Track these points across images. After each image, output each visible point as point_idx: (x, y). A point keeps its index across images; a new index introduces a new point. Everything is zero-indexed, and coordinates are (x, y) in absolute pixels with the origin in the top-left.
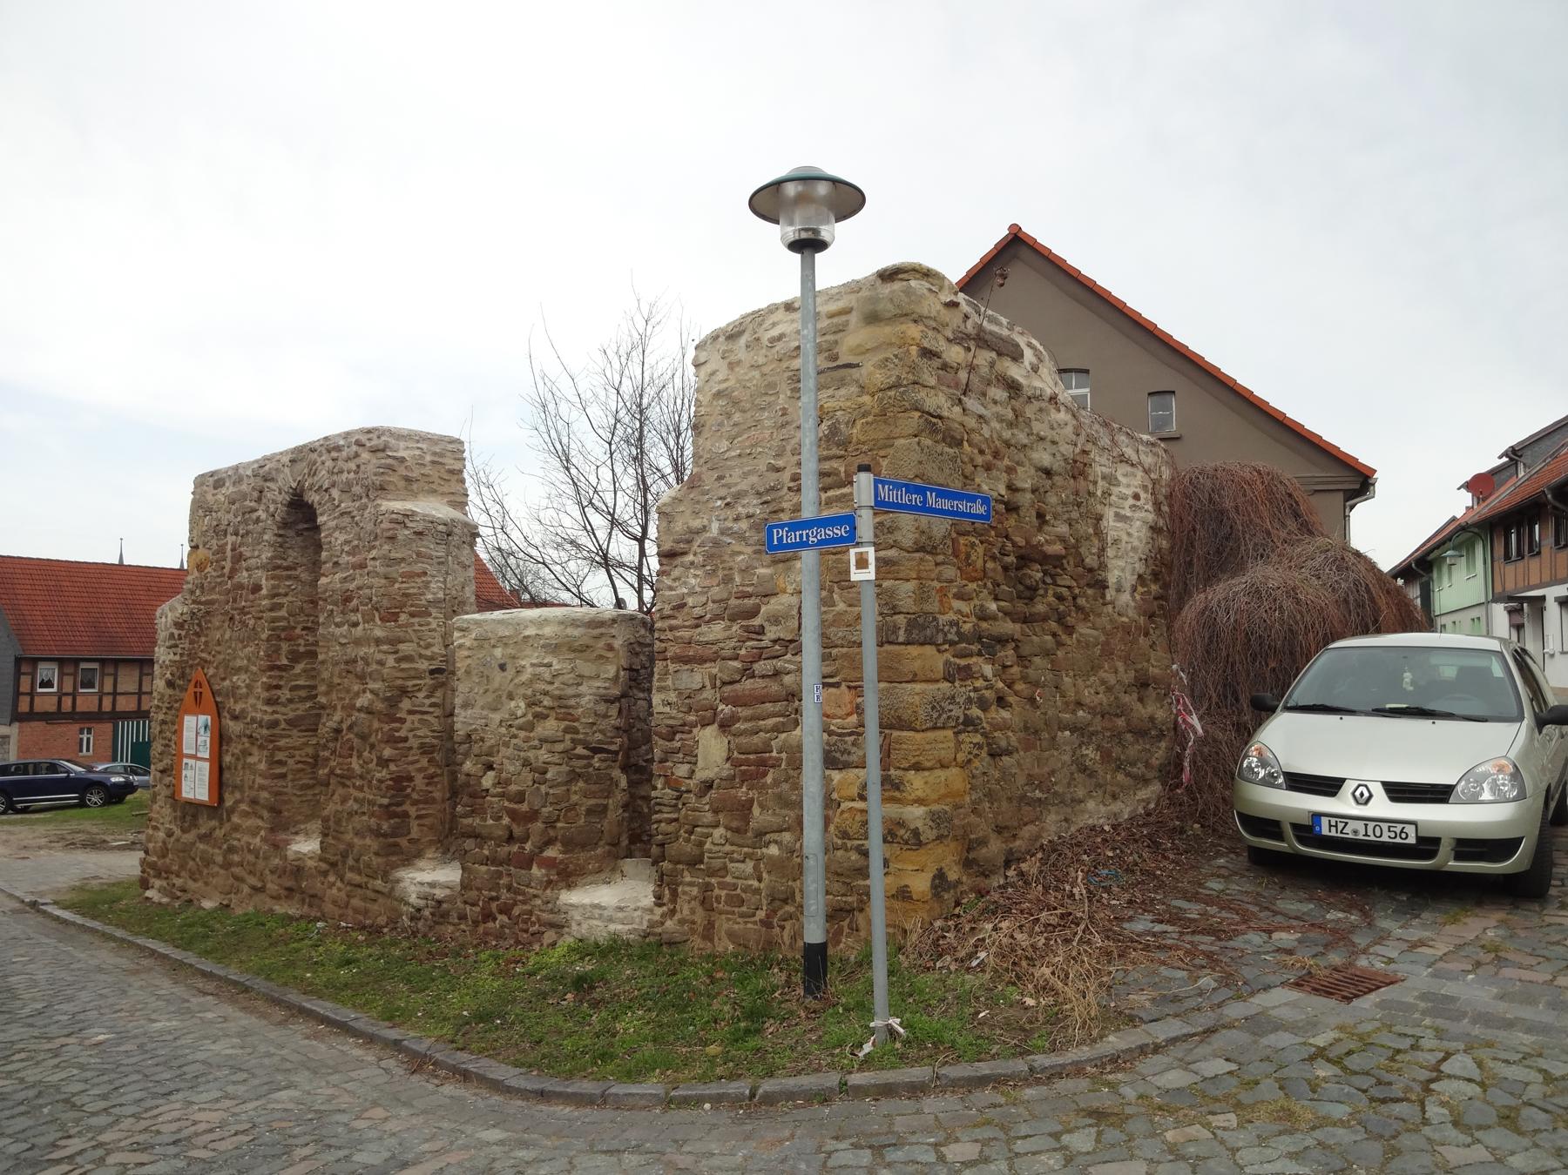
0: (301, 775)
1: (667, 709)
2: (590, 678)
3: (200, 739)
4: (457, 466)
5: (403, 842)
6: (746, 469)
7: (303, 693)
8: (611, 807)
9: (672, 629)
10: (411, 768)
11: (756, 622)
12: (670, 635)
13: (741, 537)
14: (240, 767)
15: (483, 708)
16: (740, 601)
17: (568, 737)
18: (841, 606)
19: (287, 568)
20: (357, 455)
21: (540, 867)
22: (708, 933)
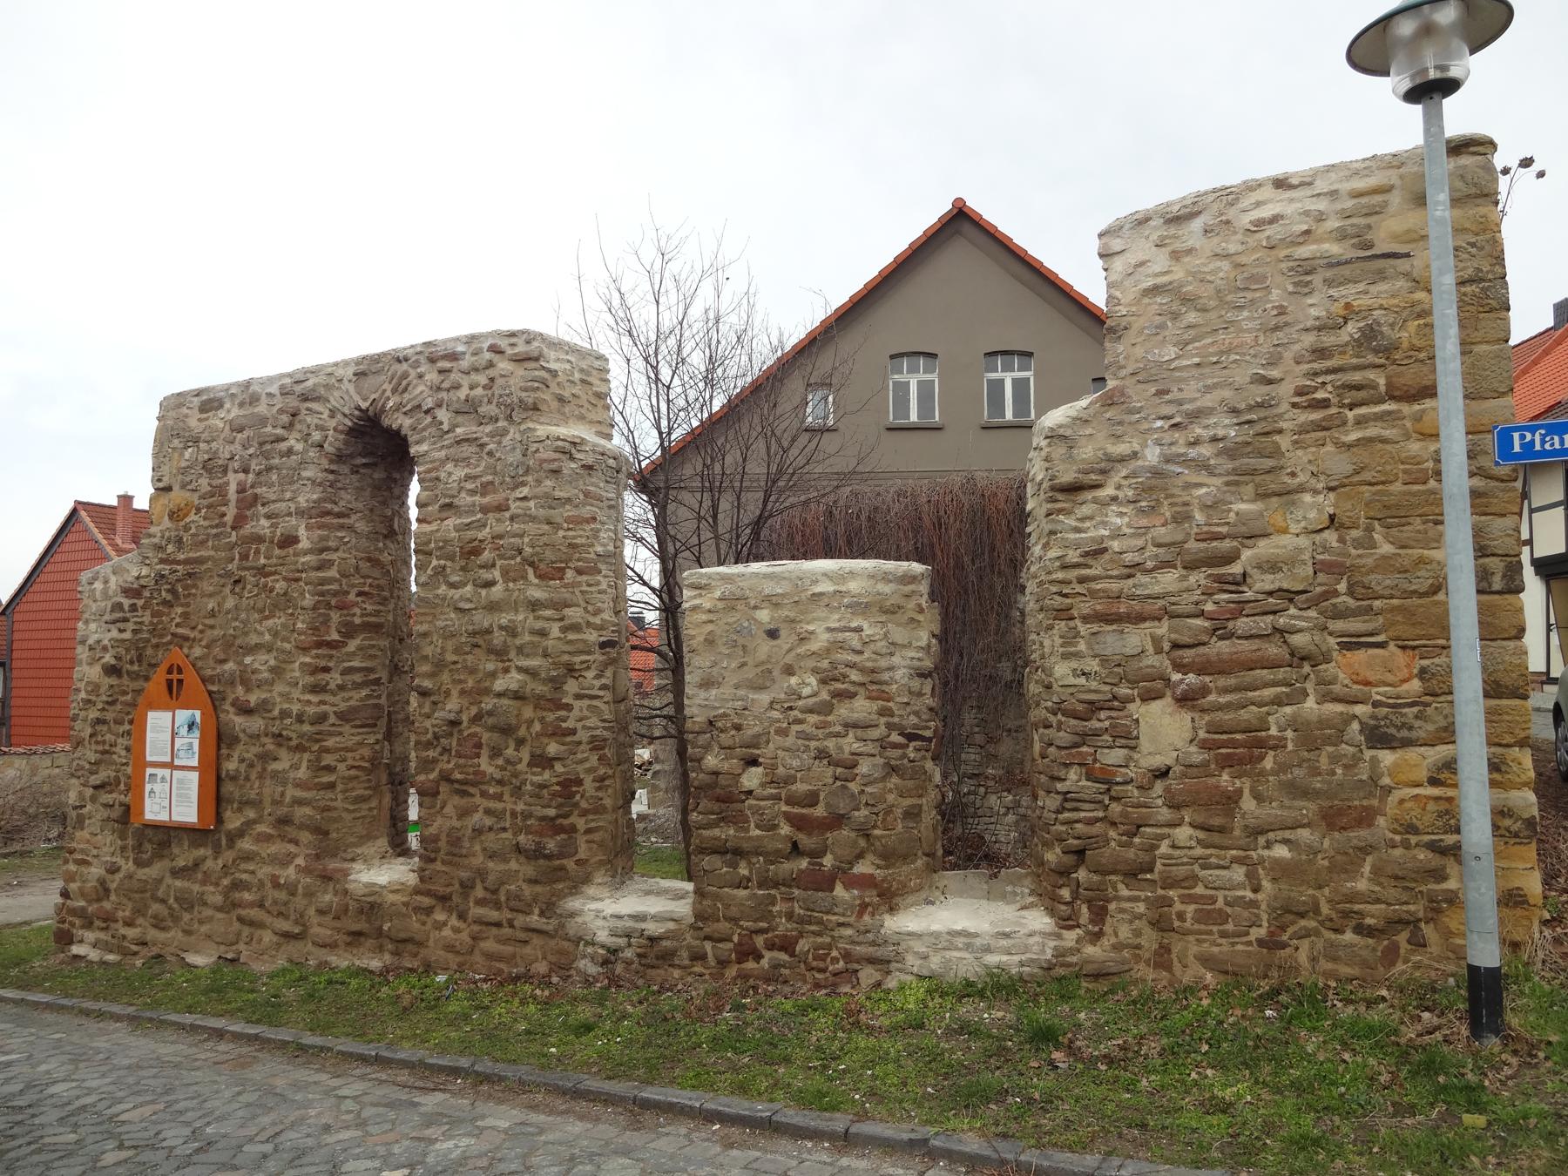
0: (354, 784)
1: (1082, 680)
2: (904, 646)
3: (178, 742)
4: (602, 389)
5: (570, 864)
6: (1209, 382)
7: (358, 678)
8: (925, 808)
9: (1082, 580)
10: (580, 768)
11: (1236, 569)
12: (1079, 588)
13: (1202, 466)
14: (253, 776)
15: (737, 687)
16: (1203, 545)
17: (883, 720)
18: (1386, 548)
19: (339, 515)
20: (491, 365)
21: (847, 887)
22: (1162, 959)
